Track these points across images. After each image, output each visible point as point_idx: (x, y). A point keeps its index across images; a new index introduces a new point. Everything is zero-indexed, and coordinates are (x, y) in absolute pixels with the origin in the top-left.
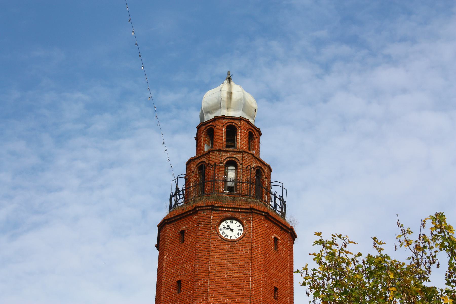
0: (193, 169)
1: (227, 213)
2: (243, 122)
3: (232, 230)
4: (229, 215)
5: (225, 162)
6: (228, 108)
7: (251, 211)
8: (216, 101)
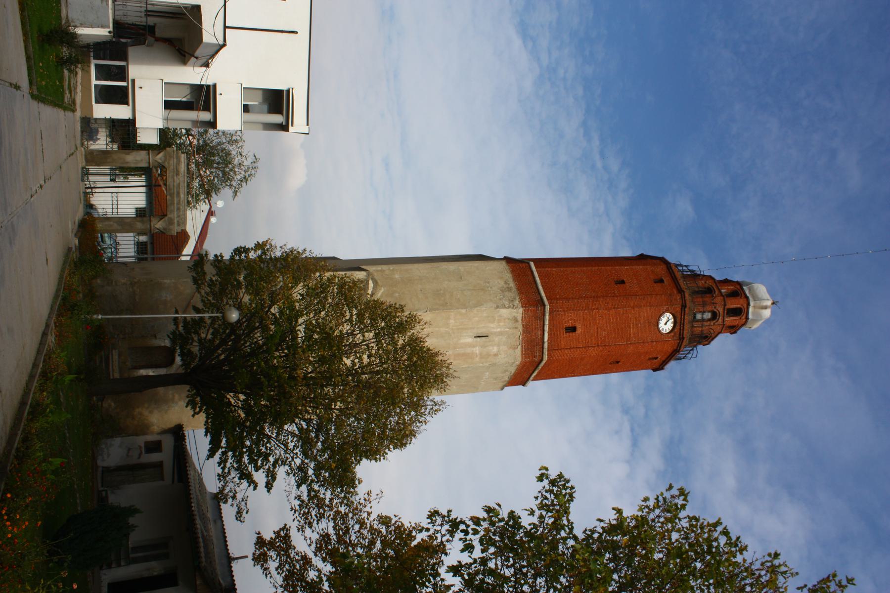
0: (707, 282)
1: (679, 318)
2: (744, 320)
3: (666, 324)
4: (678, 320)
5: (716, 310)
6: (754, 307)
7: (681, 338)
8: (760, 296)
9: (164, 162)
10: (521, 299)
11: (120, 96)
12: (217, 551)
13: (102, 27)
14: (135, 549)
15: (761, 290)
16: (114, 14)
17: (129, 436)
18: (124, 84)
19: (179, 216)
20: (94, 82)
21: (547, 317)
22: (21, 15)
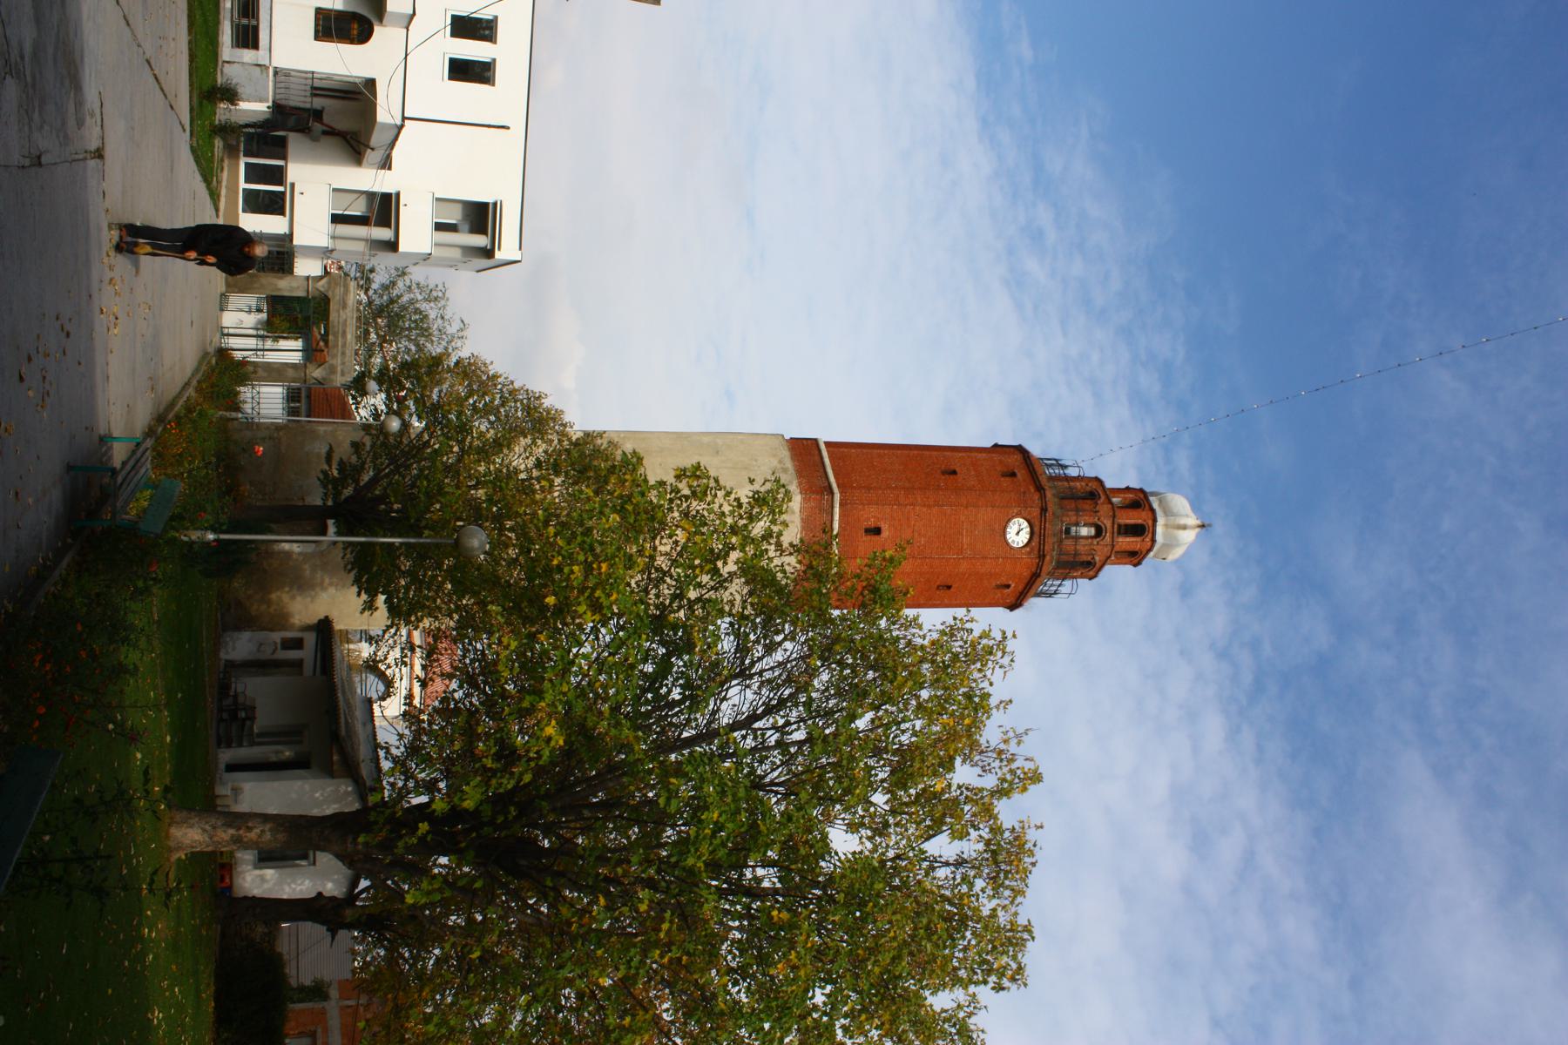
4: (1036, 529)
7: (1042, 556)
8: (1175, 511)
9: (327, 291)
10: (800, 484)
11: (274, 204)
12: (361, 732)
13: (261, 101)
14: (260, 735)
15: (1180, 503)
16: (275, 93)
17: (262, 630)
18: (280, 189)
19: (343, 363)
20: (243, 185)
21: (837, 510)
22: (190, 65)
